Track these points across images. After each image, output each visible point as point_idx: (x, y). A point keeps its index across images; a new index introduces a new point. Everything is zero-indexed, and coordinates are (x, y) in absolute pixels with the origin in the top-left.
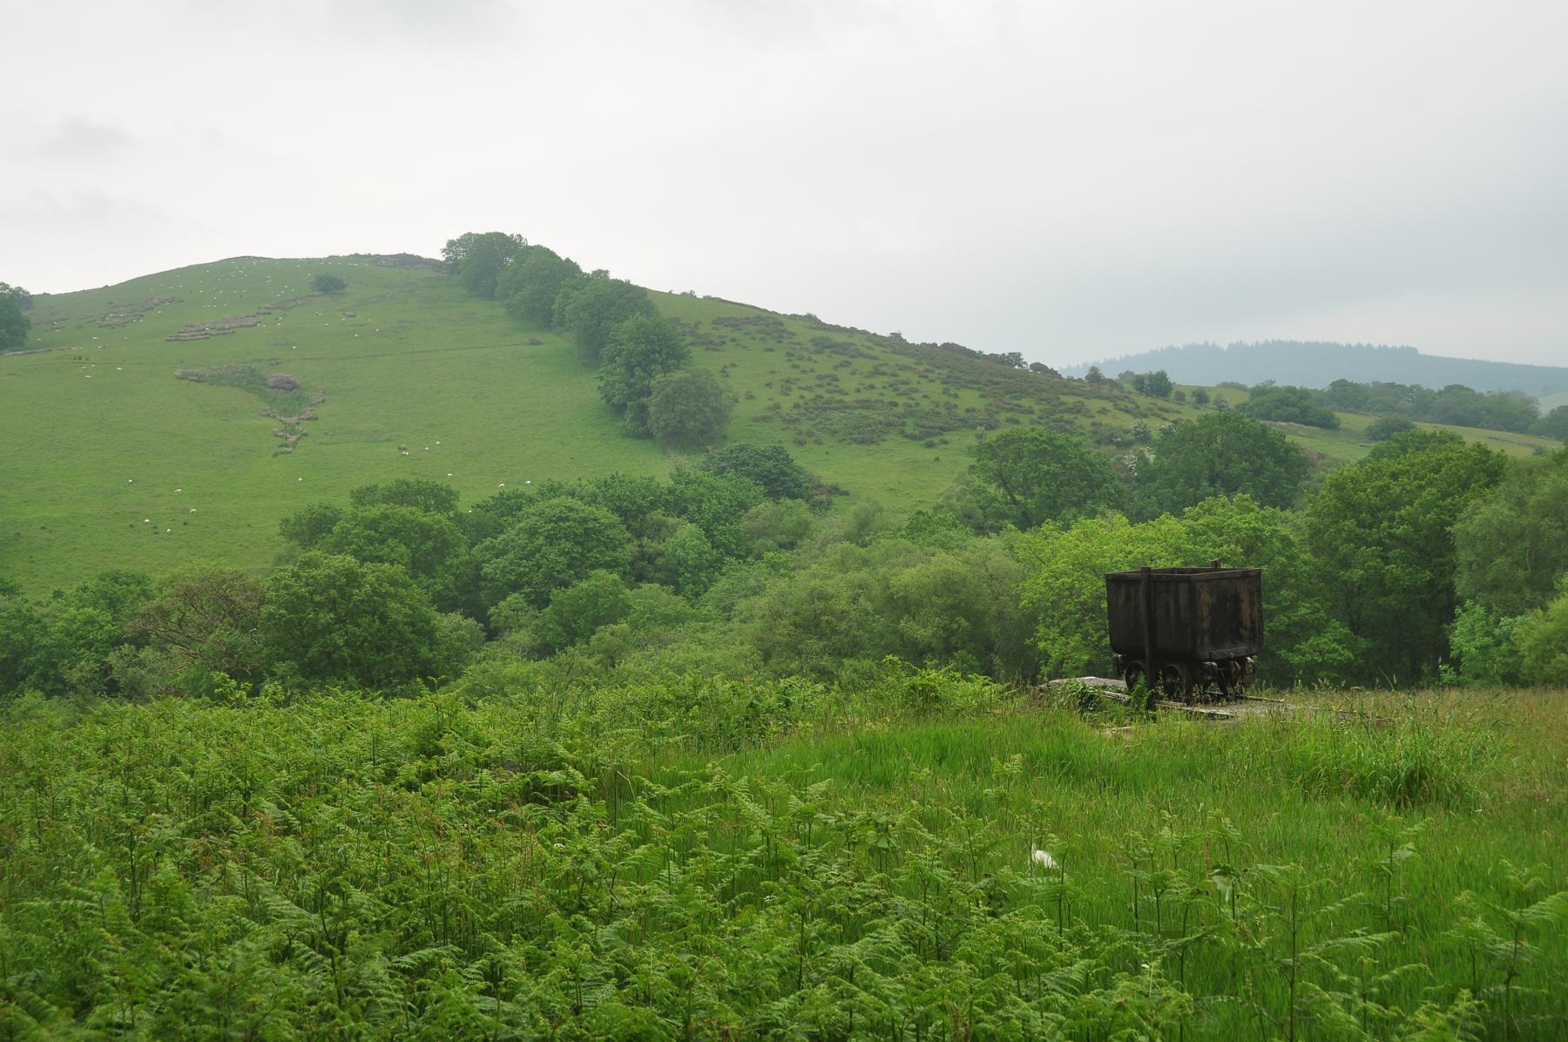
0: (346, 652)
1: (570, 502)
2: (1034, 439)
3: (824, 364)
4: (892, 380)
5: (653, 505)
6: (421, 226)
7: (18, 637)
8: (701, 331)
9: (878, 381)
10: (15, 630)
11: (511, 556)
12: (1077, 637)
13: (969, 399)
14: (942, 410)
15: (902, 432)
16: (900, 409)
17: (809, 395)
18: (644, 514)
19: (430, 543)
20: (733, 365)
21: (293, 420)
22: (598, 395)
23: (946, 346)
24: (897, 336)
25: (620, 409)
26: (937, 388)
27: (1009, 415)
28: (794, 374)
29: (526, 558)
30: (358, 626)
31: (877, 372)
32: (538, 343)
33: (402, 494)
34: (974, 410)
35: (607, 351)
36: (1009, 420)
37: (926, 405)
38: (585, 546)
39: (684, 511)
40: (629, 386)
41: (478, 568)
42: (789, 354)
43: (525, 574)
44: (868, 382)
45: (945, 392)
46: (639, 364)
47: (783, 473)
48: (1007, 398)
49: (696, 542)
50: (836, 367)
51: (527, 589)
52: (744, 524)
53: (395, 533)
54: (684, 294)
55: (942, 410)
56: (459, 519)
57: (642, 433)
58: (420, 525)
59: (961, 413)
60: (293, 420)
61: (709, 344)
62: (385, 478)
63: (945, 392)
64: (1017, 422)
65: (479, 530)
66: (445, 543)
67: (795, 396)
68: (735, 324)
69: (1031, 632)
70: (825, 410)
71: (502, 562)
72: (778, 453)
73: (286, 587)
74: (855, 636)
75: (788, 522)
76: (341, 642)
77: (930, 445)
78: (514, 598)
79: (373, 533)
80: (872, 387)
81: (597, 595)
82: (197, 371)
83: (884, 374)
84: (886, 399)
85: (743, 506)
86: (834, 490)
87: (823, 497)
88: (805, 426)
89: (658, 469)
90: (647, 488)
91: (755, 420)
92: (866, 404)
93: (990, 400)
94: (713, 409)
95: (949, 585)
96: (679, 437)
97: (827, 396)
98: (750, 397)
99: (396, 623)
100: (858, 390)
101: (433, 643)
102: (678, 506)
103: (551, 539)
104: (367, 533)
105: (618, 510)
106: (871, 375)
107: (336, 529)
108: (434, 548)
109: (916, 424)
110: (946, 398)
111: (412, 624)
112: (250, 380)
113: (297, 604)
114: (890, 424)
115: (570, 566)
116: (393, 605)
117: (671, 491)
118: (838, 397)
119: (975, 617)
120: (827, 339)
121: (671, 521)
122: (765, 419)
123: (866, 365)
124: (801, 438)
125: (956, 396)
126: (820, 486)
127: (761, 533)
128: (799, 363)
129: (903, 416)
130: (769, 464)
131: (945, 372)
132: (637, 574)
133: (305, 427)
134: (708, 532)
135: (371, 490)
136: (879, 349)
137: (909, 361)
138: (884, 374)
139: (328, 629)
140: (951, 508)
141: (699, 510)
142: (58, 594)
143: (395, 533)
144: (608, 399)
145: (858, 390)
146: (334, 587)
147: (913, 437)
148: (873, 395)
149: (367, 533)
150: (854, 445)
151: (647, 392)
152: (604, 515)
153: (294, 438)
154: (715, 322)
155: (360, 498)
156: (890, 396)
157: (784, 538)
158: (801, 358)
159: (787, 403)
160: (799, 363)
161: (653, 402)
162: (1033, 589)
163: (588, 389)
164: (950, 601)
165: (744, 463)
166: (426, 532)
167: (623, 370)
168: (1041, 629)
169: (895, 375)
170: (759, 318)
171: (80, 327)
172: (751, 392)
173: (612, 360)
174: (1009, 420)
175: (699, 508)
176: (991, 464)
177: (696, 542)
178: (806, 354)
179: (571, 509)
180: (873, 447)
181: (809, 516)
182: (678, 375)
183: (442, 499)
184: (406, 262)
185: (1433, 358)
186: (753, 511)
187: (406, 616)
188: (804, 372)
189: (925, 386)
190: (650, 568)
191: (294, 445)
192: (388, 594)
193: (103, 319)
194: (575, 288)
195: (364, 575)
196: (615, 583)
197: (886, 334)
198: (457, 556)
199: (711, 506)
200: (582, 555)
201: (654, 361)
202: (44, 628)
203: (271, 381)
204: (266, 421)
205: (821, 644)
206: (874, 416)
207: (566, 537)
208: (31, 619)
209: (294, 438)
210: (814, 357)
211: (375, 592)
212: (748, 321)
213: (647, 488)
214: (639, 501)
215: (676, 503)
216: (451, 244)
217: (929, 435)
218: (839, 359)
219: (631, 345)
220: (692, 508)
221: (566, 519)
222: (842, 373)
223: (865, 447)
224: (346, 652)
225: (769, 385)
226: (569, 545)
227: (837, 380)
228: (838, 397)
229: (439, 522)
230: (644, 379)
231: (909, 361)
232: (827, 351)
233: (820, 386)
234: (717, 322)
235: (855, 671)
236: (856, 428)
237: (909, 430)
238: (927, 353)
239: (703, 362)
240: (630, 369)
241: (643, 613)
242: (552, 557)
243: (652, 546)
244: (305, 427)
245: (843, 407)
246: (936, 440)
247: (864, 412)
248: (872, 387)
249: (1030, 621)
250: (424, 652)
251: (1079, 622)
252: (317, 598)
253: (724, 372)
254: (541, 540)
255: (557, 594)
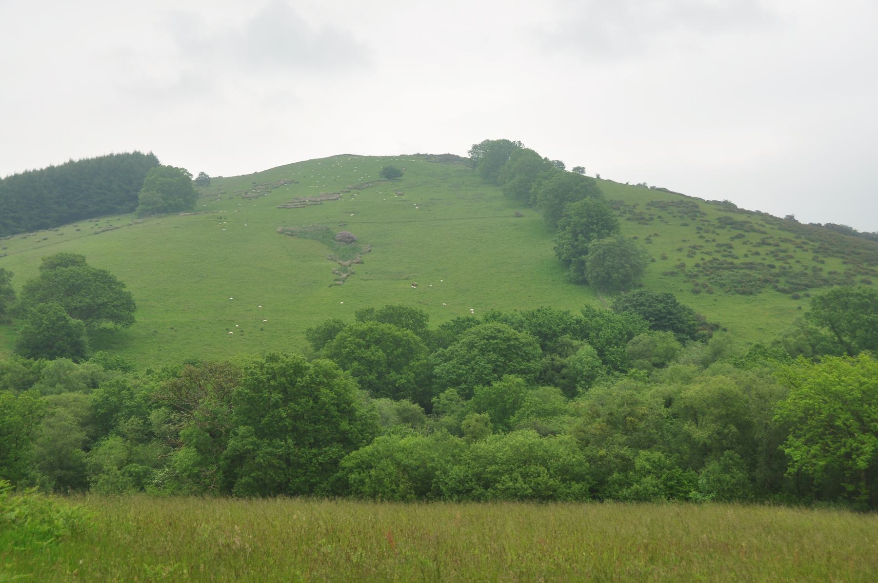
0: (288, 422)
1: (499, 325)
2: (858, 295)
3: (724, 236)
4: (773, 249)
5: (564, 331)
6: (452, 134)
7: (114, 399)
8: (637, 211)
9: (762, 250)
10: (113, 394)
11: (454, 362)
12: (817, 447)
13: (834, 265)
14: (809, 272)
15: (775, 287)
16: (777, 271)
17: (708, 258)
18: (558, 337)
19: (400, 350)
20: (656, 235)
21: (347, 263)
22: (554, 253)
23: (829, 226)
24: (790, 218)
25: (567, 263)
26: (810, 255)
27: (863, 277)
28: (701, 242)
29: (466, 363)
30: (299, 404)
31: (764, 243)
32: (521, 216)
33: (392, 315)
34: (835, 273)
35: (561, 222)
36: (862, 281)
37: (797, 268)
38: (505, 355)
39: (587, 336)
40: (574, 247)
41: (432, 368)
42: (699, 228)
43: (463, 375)
44: (754, 250)
45: (815, 259)
46: (582, 232)
47: (670, 313)
48: (865, 265)
49: (590, 359)
50: (732, 239)
51: (463, 386)
52: (629, 347)
53: (377, 342)
54: (639, 185)
55: (809, 272)
56: (426, 336)
57: (581, 282)
58: (394, 337)
59: (824, 275)
60: (347, 263)
61: (641, 219)
62: (379, 306)
63: (815, 259)
64: (869, 283)
65: (438, 342)
66: (411, 351)
67: (697, 259)
68: (663, 206)
69: (783, 440)
70: (718, 269)
71: (448, 365)
72: (668, 298)
73: (252, 374)
74: (650, 434)
75: (661, 347)
76: (284, 415)
77: (796, 298)
78: (451, 392)
79: (361, 341)
80: (757, 254)
81: (505, 392)
82: (292, 228)
83: (769, 244)
84: (766, 263)
85: (631, 335)
86: (715, 327)
87: (706, 332)
88: (702, 280)
89: (574, 304)
90: (561, 319)
91: (665, 274)
92: (751, 266)
93: (850, 266)
94: (632, 266)
95: (724, 399)
96: (606, 284)
97: (722, 259)
98: (664, 258)
99: (325, 404)
100: (746, 256)
101: (352, 420)
102: (582, 332)
103: (483, 351)
104: (357, 340)
105: (540, 334)
106: (758, 245)
107: (338, 337)
108: (402, 354)
109: (787, 282)
110: (814, 264)
111: (338, 405)
112: (325, 236)
113: (257, 386)
114: (766, 281)
115: (494, 371)
116: (324, 390)
117: (578, 322)
118: (729, 260)
119: (745, 426)
120: (731, 218)
121: (576, 343)
122: (672, 274)
123: (757, 238)
124: (697, 288)
125: (823, 262)
126: (705, 324)
127: (641, 355)
128: (705, 235)
129: (778, 275)
130: (660, 306)
131: (817, 244)
132: (543, 378)
133: (355, 268)
134: (601, 353)
135: (370, 311)
136: (768, 226)
137: (791, 236)
138: (769, 244)
139: (276, 406)
140: (786, 344)
141: (597, 336)
142: (149, 372)
143: (377, 342)
144: (559, 255)
145: (746, 256)
146: (285, 376)
147: (783, 291)
148: (757, 260)
149: (357, 340)
150: (737, 296)
151: (585, 252)
152: (524, 336)
153: (344, 275)
154: (649, 204)
155: (362, 316)
156: (771, 260)
157: (656, 360)
158: (707, 232)
159: (690, 263)
160: (705, 235)
161: (589, 258)
162: (787, 406)
163: (547, 250)
164: (724, 412)
165: (642, 304)
166: (397, 342)
167: (570, 235)
168: (791, 437)
169: (777, 245)
170: (681, 202)
171: (231, 198)
172: (663, 256)
173: (564, 228)
174: (862, 281)
175: (597, 335)
176: (823, 312)
177: (590, 359)
178: (711, 229)
179: (499, 331)
180: (751, 297)
181: (677, 345)
182: (608, 240)
183: (417, 321)
184: (448, 159)
185: (100, 160)
186: (636, 338)
187: (333, 399)
188: (707, 241)
189: (800, 255)
190: (557, 376)
191: (344, 280)
192: (320, 383)
193: (246, 193)
194: (546, 178)
195: (307, 368)
196: (518, 385)
197: (783, 216)
198: (418, 360)
199: (606, 333)
200: (504, 363)
201: (593, 230)
202: (132, 394)
203: (338, 236)
204: (331, 263)
205: (625, 437)
206: (755, 274)
207: (494, 350)
208: (124, 388)
209: (344, 275)
210: (718, 231)
211: (313, 382)
212: (673, 204)
213: (561, 319)
214: (554, 327)
215: (582, 331)
216: (475, 147)
217: (796, 290)
218: (736, 232)
219: (576, 219)
220: (592, 334)
221: (495, 338)
222: (736, 243)
223: (746, 297)
224: (288, 422)
225: (680, 250)
226: (495, 356)
227: (731, 247)
228: (729, 260)
229: (407, 335)
230: (584, 242)
231: (791, 236)
232: (728, 227)
233: (718, 252)
234: (651, 204)
235: (648, 460)
236: (740, 282)
237: (781, 286)
238: (813, 231)
239: (628, 230)
240: (575, 234)
241: (529, 407)
242: (482, 364)
243: (559, 360)
244: (355, 268)
245: (733, 267)
246: (801, 294)
247: (747, 271)
248: (757, 254)
249: (782, 432)
250: (344, 425)
251: (821, 436)
252: (272, 383)
253: (648, 240)
254: (476, 352)
255: (479, 389)
